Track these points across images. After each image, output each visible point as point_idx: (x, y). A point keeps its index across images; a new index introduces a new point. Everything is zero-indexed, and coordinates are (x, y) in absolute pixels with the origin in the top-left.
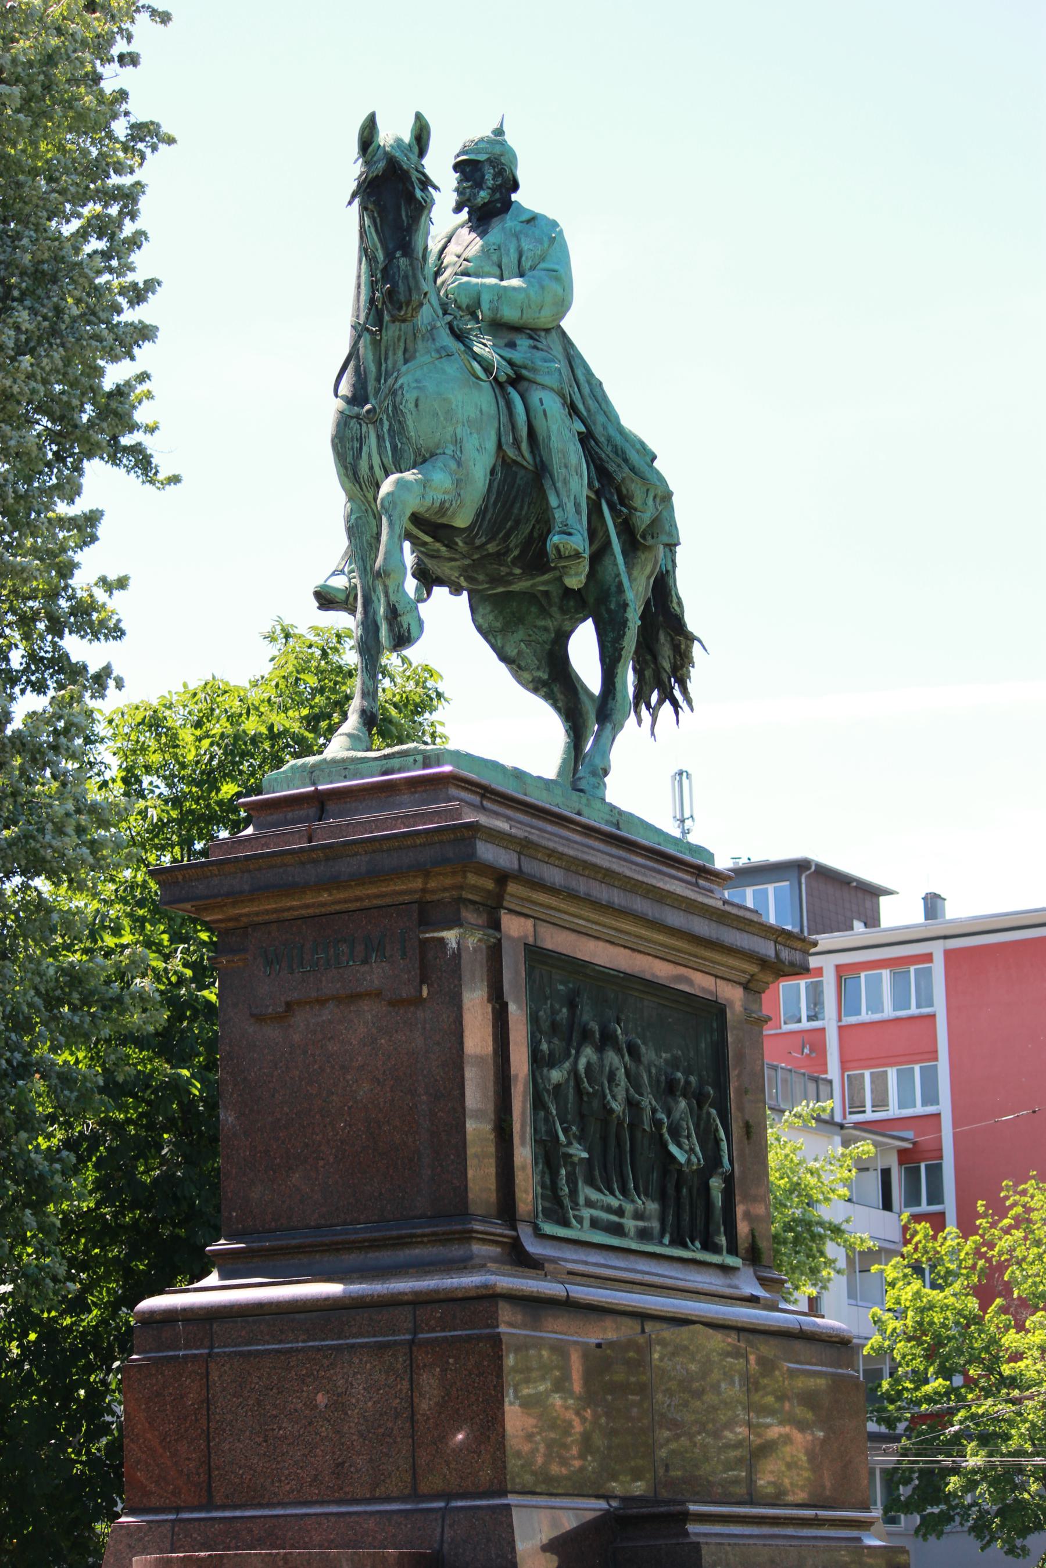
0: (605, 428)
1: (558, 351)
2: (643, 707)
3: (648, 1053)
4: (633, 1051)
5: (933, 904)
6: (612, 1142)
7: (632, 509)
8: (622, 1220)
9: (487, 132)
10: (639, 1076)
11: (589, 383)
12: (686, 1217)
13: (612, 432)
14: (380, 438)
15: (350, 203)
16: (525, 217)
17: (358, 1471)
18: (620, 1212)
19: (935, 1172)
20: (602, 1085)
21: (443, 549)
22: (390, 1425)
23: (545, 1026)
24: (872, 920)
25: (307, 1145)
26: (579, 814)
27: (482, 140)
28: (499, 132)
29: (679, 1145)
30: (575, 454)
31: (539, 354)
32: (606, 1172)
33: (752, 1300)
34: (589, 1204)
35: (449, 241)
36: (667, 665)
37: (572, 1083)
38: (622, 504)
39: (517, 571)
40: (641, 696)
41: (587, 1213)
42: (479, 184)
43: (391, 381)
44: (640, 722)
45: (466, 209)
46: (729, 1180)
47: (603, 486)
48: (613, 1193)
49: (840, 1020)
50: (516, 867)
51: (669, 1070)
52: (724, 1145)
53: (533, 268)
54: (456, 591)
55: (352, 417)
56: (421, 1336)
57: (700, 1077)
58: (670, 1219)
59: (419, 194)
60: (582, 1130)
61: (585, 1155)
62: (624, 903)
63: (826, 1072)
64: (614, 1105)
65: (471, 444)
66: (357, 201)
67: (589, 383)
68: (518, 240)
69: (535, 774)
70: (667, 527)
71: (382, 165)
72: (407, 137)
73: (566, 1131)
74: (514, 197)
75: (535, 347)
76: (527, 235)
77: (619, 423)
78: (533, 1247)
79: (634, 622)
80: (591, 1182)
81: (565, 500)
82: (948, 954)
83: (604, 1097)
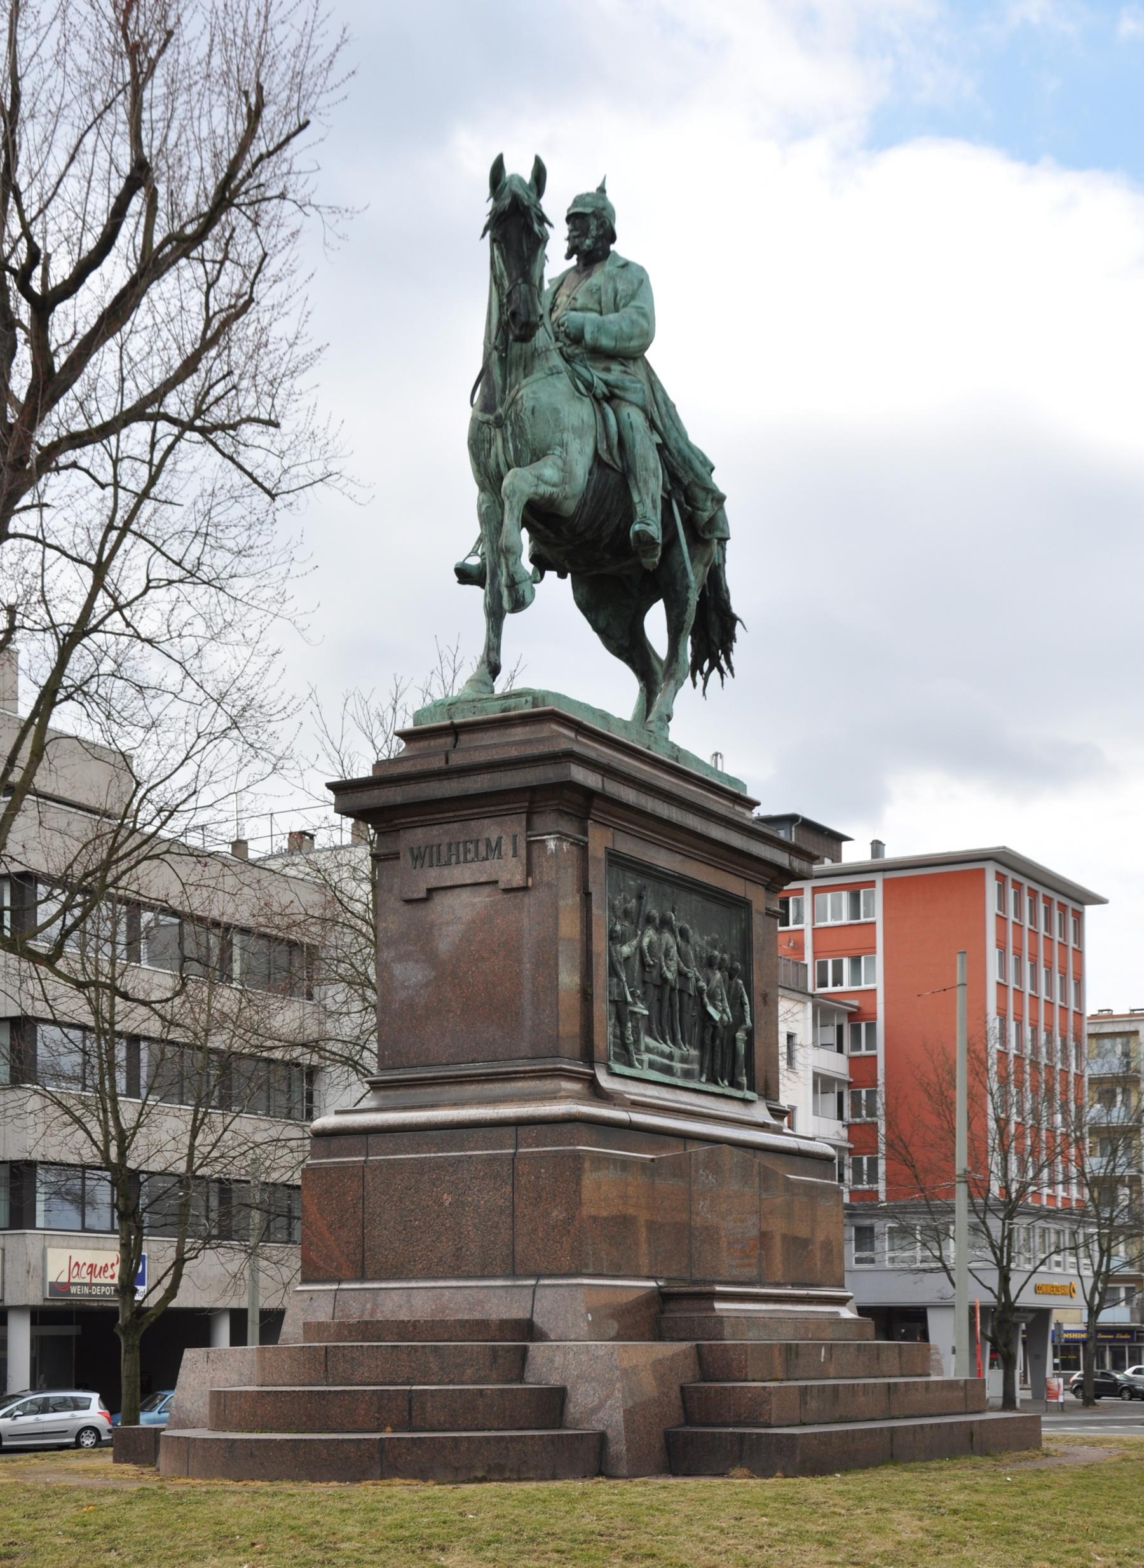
0: (677, 442)
1: (642, 375)
2: (698, 673)
3: (694, 936)
4: (683, 933)
5: (877, 847)
6: (666, 1004)
7: (696, 508)
8: (673, 1064)
9: (593, 189)
10: (687, 953)
11: (666, 405)
12: (718, 1061)
13: (682, 445)
14: (504, 440)
15: (483, 236)
16: (620, 263)
17: (472, 1255)
18: (670, 1057)
19: (871, 1028)
20: (660, 959)
21: (552, 535)
22: (496, 1219)
23: (619, 913)
24: (837, 858)
25: (441, 1000)
26: (649, 748)
27: (588, 195)
28: (602, 190)
29: (715, 1007)
30: (653, 461)
31: (628, 377)
32: (661, 1024)
33: (763, 1127)
34: (649, 1050)
35: (562, 284)
36: (716, 639)
37: (638, 957)
38: (688, 503)
39: (608, 556)
40: (696, 666)
41: (646, 1057)
42: (585, 233)
43: (513, 392)
44: (695, 685)
45: (575, 257)
46: (750, 1033)
47: (674, 488)
48: (665, 1042)
49: (813, 924)
50: (600, 786)
51: (709, 950)
52: (747, 1008)
53: (625, 306)
54: (562, 575)
55: (483, 423)
56: (521, 1150)
57: (732, 956)
58: (706, 1064)
59: (536, 227)
60: (644, 993)
61: (646, 1012)
62: (680, 819)
63: (803, 959)
64: (669, 975)
65: (574, 445)
66: (488, 233)
67: (666, 405)
68: (615, 281)
69: (617, 716)
70: (721, 524)
71: (507, 201)
72: (527, 177)
73: (632, 994)
74: (612, 247)
75: (625, 372)
76: (621, 278)
77: (687, 439)
78: (605, 1082)
79: (694, 597)
80: (650, 1034)
81: (645, 497)
82: (886, 882)
83: (661, 968)
